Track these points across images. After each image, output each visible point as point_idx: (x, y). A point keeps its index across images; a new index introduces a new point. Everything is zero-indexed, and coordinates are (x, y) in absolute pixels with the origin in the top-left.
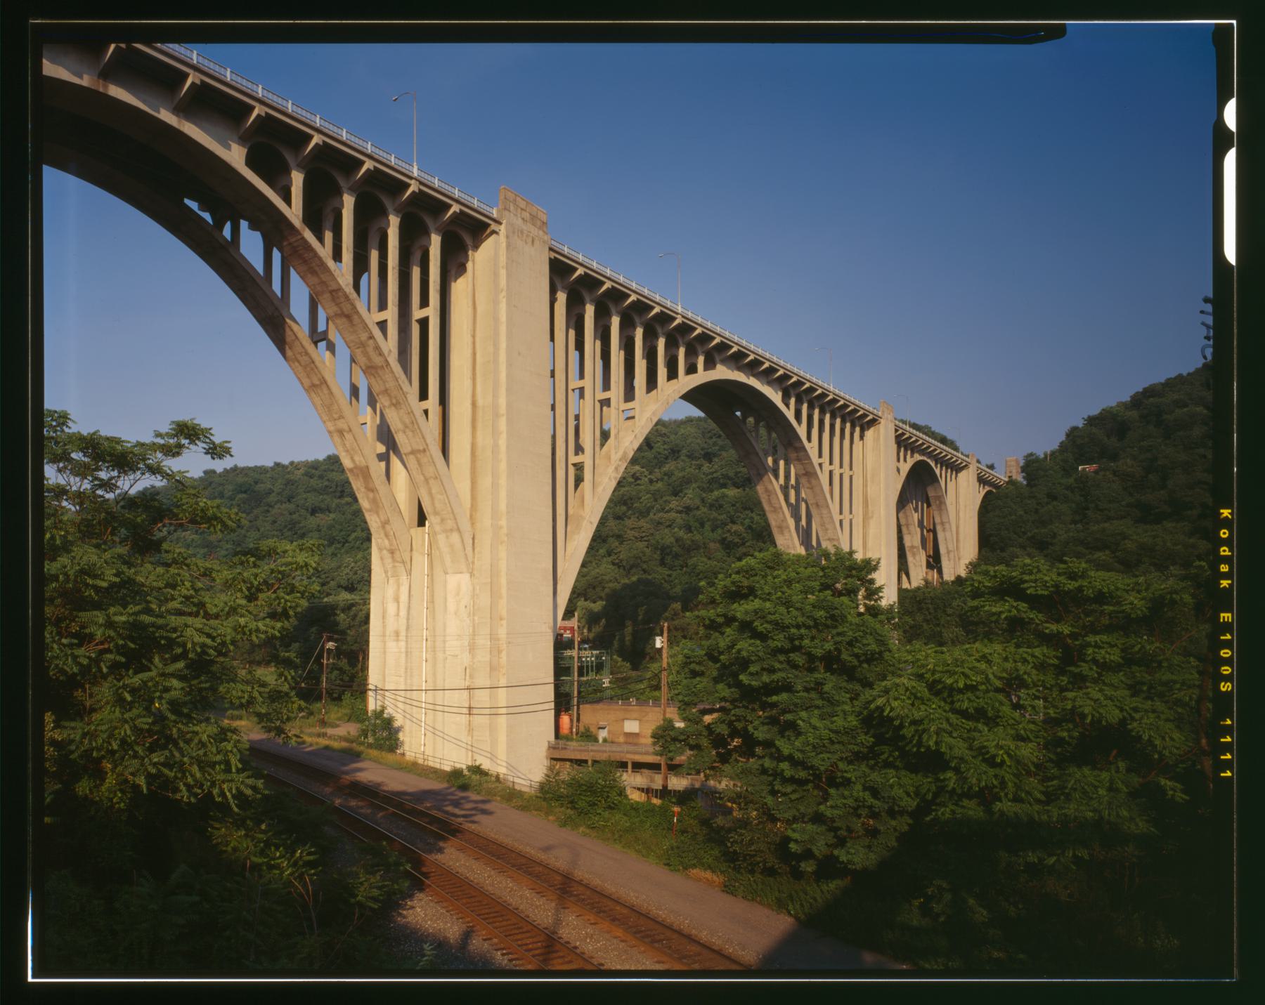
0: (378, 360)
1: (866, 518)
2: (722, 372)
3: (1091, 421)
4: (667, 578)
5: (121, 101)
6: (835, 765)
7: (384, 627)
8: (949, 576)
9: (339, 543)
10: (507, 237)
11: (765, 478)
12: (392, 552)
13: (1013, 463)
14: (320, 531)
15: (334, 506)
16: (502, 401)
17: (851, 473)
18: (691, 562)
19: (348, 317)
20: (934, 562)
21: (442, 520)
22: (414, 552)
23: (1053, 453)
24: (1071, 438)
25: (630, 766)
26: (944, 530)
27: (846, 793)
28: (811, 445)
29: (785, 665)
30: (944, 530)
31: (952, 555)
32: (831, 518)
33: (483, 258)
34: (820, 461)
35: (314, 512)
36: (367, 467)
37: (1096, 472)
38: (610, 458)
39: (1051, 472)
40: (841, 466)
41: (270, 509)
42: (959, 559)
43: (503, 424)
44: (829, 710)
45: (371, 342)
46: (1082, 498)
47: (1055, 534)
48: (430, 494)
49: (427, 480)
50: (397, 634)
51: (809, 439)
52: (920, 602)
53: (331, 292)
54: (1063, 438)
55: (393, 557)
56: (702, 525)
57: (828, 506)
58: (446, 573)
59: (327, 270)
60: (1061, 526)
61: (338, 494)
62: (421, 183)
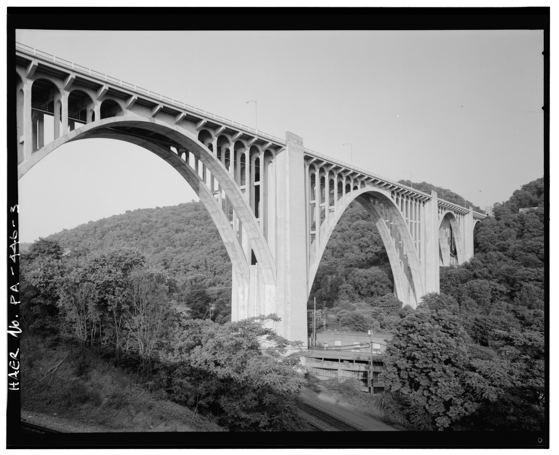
0: (242, 205)
1: (426, 241)
2: (369, 188)
3: (525, 187)
4: (335, 262)
5: (159, 125)
6: (451, 399)
7: (238, 304)
8: (461, 263)
9: (189, 246)
10: (289, 151)
11: (380, 220)
12: (242, 275)
13: (489, 208)
14: (180, 240)
15: (186, 228)
16: (288, 216)
17: (419, 222)
18: (346, 255)
19: (232, 190)
20: (454, 253)
21: (264, 264)
22: (251, 275)
23: (507, 202)
24: (515, 195)
25: (339, 361)
26: (458, 241)
27: (456, 409)
28: (403, 213)
29: (431, 362)
30: (458, 241)
31: (462, 252)
32: (411, 243)
33: (279, 158)
34: (407, 219)
35: (177, 231)
36: (233, 243)
37: (527, 213)
38: (325, 230)
39: (506, 212)
40: (415, 220)
41: (157, 230)
42: (465, 253)
43: (288, 226)
44: (448, 379)
45: (240, 199)
46: (521, 225)
47: (509, 244)
48: (260, 254)
49: (259, 249)
50: (244, 307)
51: (402, 210)
52: (449, 276)
53: (226, 181)
54: (512, 195)
55: (242, 277)
56: (350, 238)
57: (410, 238)
58: (265, 284)
59: (224, 172)
60: (511, 240)
61: (187, 223)
62: (258, 136)
